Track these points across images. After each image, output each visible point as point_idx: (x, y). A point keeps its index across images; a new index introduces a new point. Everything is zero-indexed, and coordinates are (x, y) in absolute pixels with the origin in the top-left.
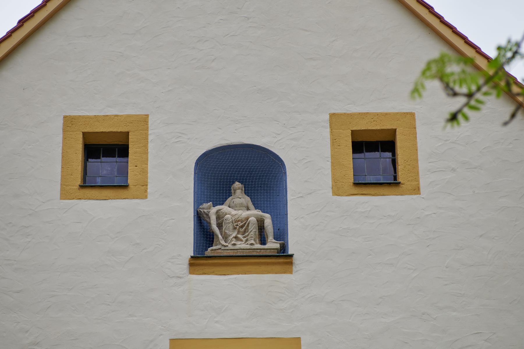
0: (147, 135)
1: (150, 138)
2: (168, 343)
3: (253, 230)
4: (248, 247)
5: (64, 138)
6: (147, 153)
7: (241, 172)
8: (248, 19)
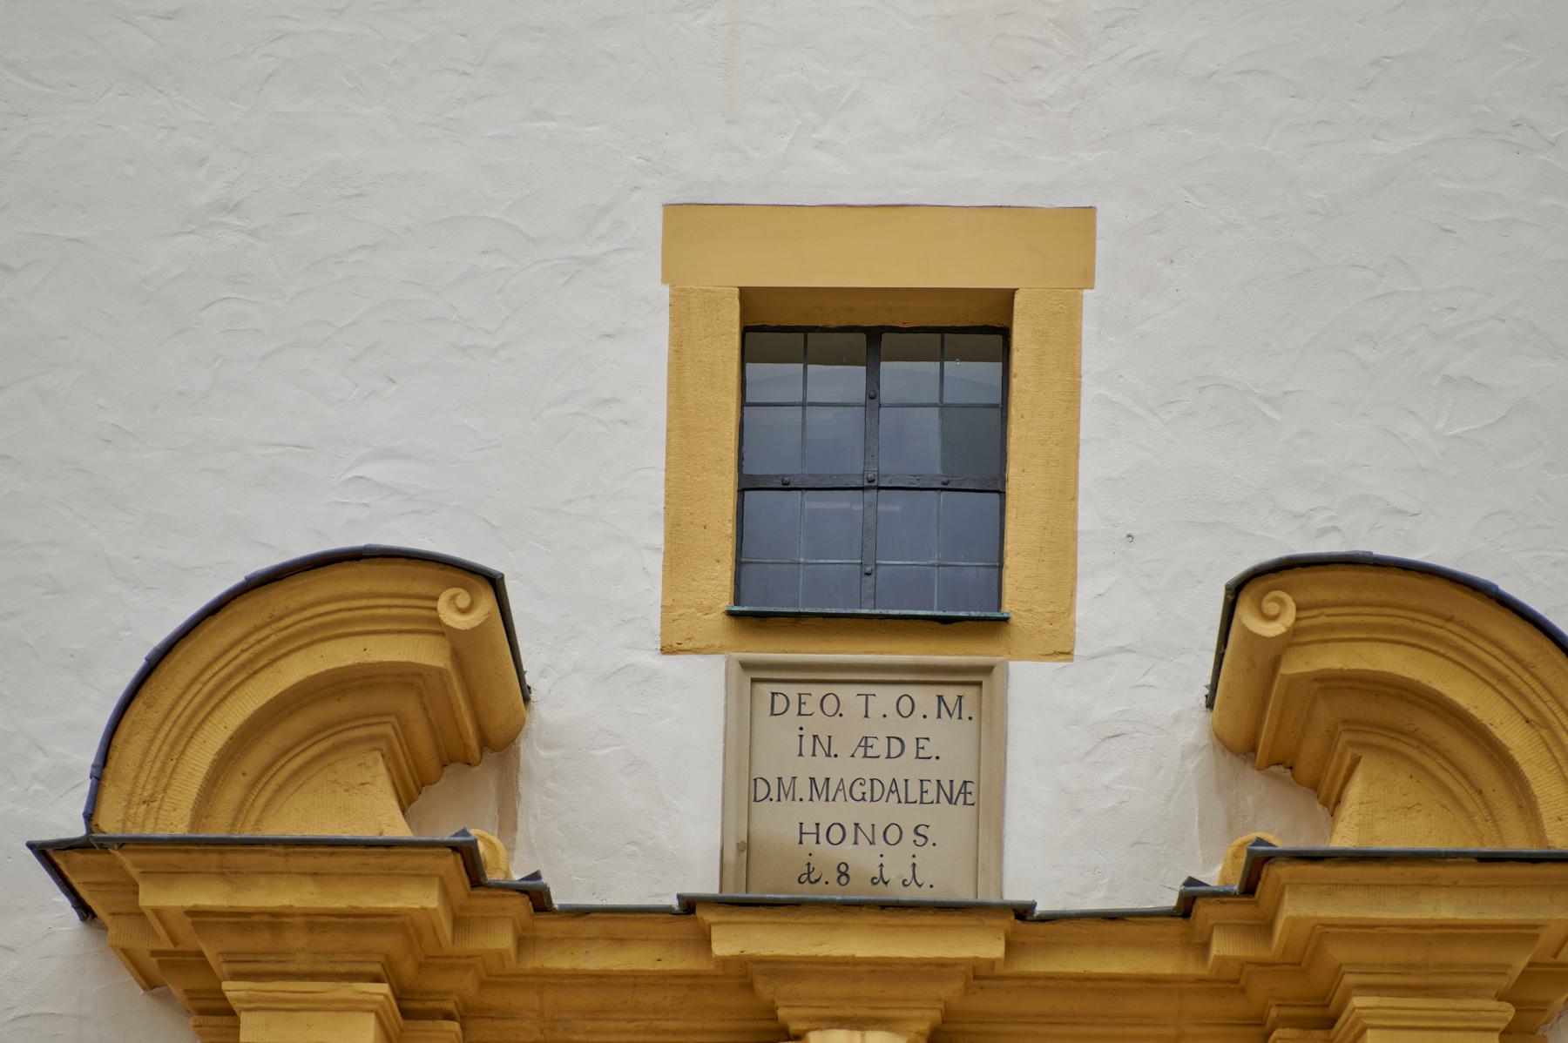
2: (661, 211)
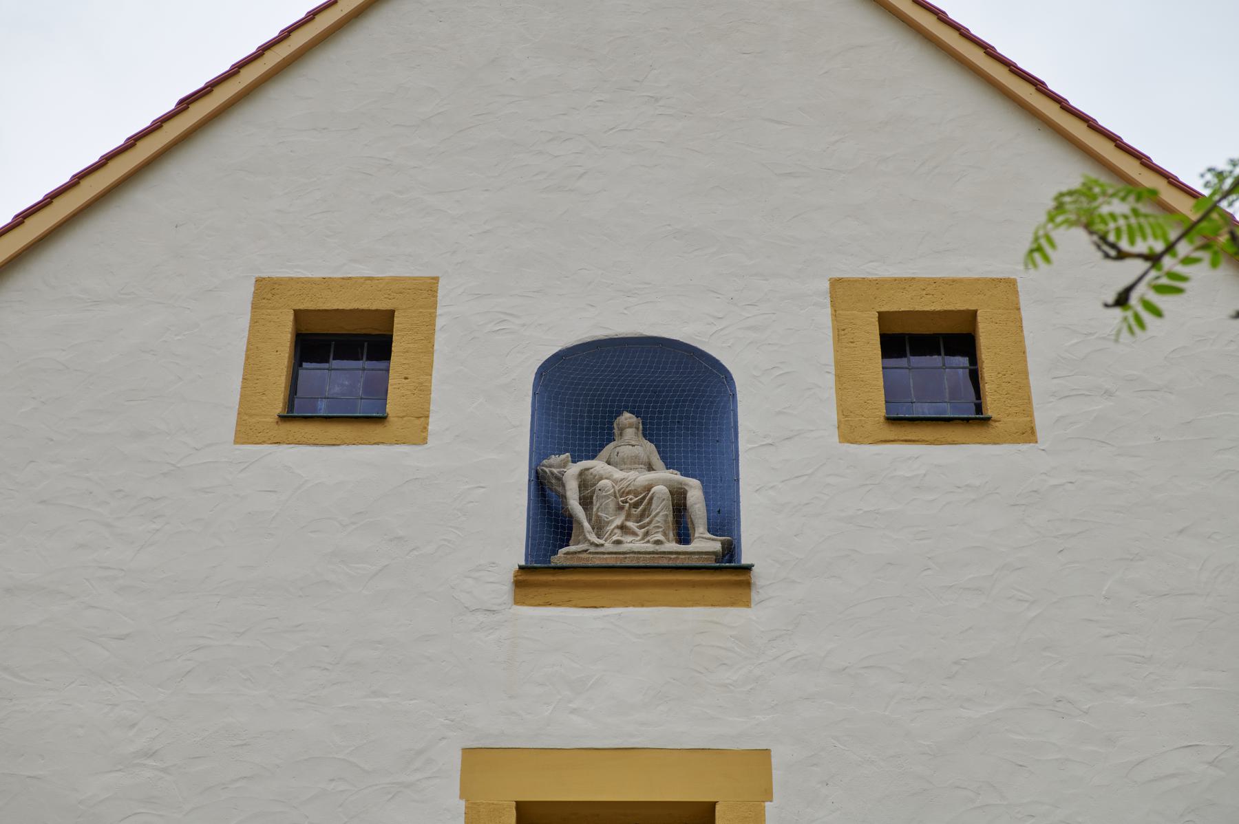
0: (433, 317)
1: (440, 322)
2: (457, 757)
3: (661, 512)
4: (650, 547)
5: (254, 322)
6: (429, 350)
7: (638, 396)
8: (657, 100)
